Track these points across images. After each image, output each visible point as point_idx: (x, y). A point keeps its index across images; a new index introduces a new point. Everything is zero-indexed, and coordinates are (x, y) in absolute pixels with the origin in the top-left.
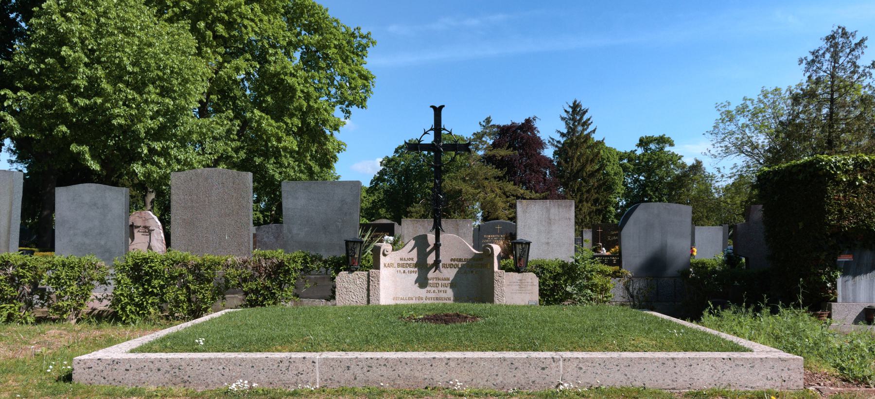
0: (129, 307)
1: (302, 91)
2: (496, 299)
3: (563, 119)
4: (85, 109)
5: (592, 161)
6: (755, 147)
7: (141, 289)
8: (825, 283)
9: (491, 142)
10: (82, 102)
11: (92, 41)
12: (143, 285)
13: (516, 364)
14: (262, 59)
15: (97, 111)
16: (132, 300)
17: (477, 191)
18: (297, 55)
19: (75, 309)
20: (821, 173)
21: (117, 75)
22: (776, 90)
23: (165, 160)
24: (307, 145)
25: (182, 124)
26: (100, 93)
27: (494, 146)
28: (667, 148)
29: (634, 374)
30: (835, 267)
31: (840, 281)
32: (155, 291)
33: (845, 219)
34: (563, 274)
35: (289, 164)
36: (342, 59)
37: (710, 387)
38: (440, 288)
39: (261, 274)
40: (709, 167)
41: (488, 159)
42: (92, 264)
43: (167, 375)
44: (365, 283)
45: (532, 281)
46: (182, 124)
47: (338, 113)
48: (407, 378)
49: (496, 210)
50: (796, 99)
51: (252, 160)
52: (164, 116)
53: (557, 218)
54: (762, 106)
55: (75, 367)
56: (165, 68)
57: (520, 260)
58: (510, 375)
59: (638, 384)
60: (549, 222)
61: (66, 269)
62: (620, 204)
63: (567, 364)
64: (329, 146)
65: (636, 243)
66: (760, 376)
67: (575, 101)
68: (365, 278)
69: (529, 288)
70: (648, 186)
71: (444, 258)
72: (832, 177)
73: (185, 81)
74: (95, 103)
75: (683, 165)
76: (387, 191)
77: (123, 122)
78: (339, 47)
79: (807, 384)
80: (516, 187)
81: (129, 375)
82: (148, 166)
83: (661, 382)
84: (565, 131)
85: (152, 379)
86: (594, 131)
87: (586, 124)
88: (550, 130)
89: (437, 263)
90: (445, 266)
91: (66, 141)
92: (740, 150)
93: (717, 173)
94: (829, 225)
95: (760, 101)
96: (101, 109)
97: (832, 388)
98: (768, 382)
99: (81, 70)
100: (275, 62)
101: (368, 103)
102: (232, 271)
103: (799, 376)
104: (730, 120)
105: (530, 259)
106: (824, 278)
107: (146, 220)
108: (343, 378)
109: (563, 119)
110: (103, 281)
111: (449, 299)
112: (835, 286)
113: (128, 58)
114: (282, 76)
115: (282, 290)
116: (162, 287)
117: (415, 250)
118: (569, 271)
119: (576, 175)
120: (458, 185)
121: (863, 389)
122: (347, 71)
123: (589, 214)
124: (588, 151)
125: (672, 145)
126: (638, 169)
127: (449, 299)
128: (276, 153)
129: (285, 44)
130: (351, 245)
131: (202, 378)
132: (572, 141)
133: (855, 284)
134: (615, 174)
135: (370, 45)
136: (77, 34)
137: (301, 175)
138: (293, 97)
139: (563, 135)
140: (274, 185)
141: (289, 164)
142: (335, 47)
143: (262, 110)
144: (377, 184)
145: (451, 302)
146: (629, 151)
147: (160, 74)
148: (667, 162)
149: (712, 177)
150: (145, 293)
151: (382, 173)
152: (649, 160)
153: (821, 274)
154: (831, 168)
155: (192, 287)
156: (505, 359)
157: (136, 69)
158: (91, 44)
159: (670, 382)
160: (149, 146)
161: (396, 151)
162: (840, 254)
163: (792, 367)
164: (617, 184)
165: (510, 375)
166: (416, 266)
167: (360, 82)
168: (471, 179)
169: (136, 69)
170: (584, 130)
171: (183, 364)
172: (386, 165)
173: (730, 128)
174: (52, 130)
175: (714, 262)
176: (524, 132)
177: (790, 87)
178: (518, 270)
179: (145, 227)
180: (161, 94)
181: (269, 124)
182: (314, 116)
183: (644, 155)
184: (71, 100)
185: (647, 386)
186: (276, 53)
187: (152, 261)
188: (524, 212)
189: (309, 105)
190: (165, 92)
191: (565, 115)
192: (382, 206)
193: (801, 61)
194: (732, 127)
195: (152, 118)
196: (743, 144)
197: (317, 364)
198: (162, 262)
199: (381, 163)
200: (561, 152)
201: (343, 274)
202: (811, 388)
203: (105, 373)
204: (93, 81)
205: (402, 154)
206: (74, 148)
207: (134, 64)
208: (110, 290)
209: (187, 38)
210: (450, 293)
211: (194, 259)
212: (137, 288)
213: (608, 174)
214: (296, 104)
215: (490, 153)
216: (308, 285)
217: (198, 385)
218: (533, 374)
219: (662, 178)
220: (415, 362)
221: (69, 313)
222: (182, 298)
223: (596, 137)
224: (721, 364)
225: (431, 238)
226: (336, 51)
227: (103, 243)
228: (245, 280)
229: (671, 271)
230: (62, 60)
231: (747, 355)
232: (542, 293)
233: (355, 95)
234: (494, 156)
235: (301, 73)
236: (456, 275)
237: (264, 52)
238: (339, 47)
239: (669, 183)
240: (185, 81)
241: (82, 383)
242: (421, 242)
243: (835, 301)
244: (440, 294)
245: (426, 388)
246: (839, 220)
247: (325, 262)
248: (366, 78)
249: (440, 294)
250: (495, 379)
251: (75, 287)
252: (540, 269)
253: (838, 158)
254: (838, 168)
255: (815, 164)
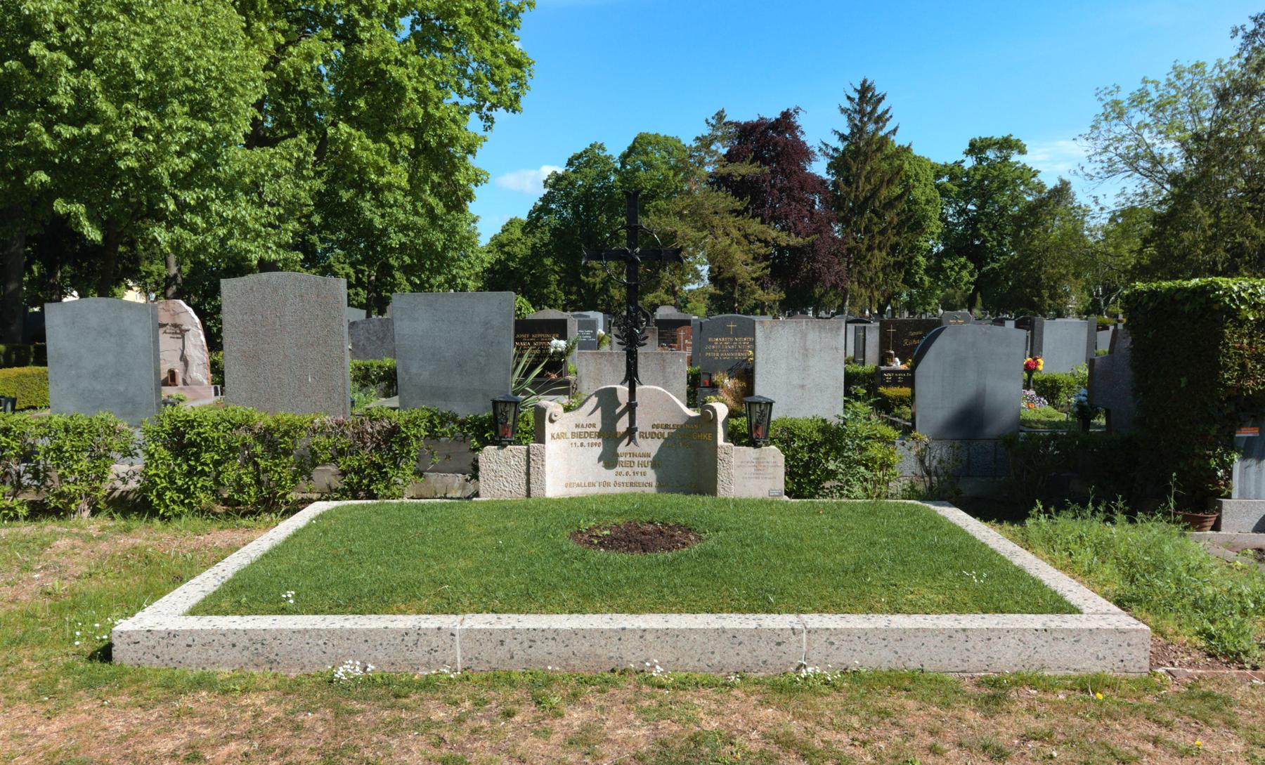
0: (168, 494)
1: (416, 90)
2: (719, 487)
3: (844, 111)
4: (73, 142)
5: (890, 182)
6: (1156, 161)
7: (185, 467)
8: (1215, 470)
9: (724, 151)
10: (67, 131)
11: (77, 28)
12: (187, 460)
13: (741, 638)
14: (348, 34)
15: (92, 145)
16: (172, 482)
17: (701, 235)
18: (405, 23)
19: (87, 495)
20: (1216, 307)
21: (120, 86)
22: (1197, 66)
23: (203, 218)
24: (426, 172)
25: (227, 161)
26: (93, 115)
27: (730, 157)
28: (1015, 158)
29: (908, 652)
30: (1231, 446)
31: (1237, 467)
32: (207, 469)
33: (1248, 377)
34: (822, 444)
35: (396, 201)
36: (479, 32)
37: (1015, 669)
38: (636, 469)
39: (365, 443)
40: (1081, 195)
41: (719, 181)
42: (108, 427)
43: (245, 653)
44: (523, 463)
45: (774, 456)
46: (227, 161)
47: (474, 124)
48: (585, 657)
49: (732, 265)
50: (1223, 97)
51: (337, 194)
52: (198, 149)
53: (818, 347)
54: (1173, 92)
55: (115, 642)
56: (196, 72)
57: (757, 428)
58: (732, 652)
59: (914, 665)
60: (806, 353)
61: (71, 436)
62: (935, 250)
63: (813, 637)
64: (460, 177)
65: (939, 388)
66: (1088, 654)
67: (865, 81)
68: (523, 456)
69: (771, 470)
70: (981, 221)
71: (642, 424)
72: (1233, 314)
73: (230, 92)
74: (89, 133)
75: (1041, 187)
76: (556, 229)
77: (136, 165)
78: (474, 13)
79: (1154, 665)
80: (764, 227)
81: (192, 653)
82: (177, 229)
83: (946, 662)
84: (847, 132)
85: (224, 658)
86: (894, 131)
87: (881, 120)
88: (822, 130)
89: (631, 432)
90: (643, 435)
91: (48, 194)
92: (1132, 162)
93: (1093, 206)
94: (1224, 386)
95: (1170, 84)
96: (94, 143)
97: (1189, 671)
98: (1098, 663)
99: (63, 79)
100: (370, 41)
101: (523, 102)
102: (322, 440)
103: (1143, 654)
104: (1120, 116)
105: (773, 418)
106: (1213, 463)
107: (176, 314)
108: (494, 657)
109: (844, 111)
110: (127, 453)
111: (650, 485)
112: (1229, 474)
113: (137, 59)
114: (383, 66)
115: (397, 467)
116: (217, 463)
117: (599, 412)
118: (832, 438)
119: (860, 208)
120: (669, 224)
121: (1234, 671)
122: (487, 54)
123: (884, 269)
124: (885, 166)
125: (1022, 151)
126: (966, 192)
127: (650, 485)
128: (377, 190)
129: (386, 9)
130: (500, 407)
131: (295, 657)
132: (858, 147)
133: (1260, 471)
134: (928, 202)
135: (526, 7)
136: (52, 18)
137: (416, 218)
138: (399, 100)
139: (843, 137)
140: (373, 235)
141: (396, 201)
142: (468, 12)
143: (349, 121)
144: (538, 218)
145: (653, 490)
146: (950, 162)
147: (190, 83)
148: (1013, 181)
149: (1086, 212)
150: (190, 473)
151: (546, 199)
152: (984, 177)
153: (1210, 457)
154: (1232, 300)
155: (262, 463)
156: (724, 631)
157: (151, 76)
158: (75, 34)
159: (959, 662)
160: (175, 197)
161: (570, 163)
162: (1241, 426)
163: (1134, 641)
164: (930, 218)
165: (732, 652)
166: (599, 435)
167: (508, 71)
168: (692, 213)
169: (151, 76)
170: (877, 130)
171: (267, 637)
172: (553, 186)
173: (1117, 130)
174: (22, 178)
175: (1071, 379)
176: (780, 133)
177: (1220, 61)
178: (754, 443)
179: (175, 326)
180: (193, 114)
181: (361, 145)
182: (435, 130)
183: (975, 169)
184: (49, 129)
185: (926, 668)
186: (372, 25)
187: (200, 425)
188: (767, 338)
189: (426, 111)
190: (199, 110)
191: (847, 104)
192: (548, 254)
193: (1235, 32)
194: (1121, 129)
195: (179, 154)
196: (1137, 157)
197: (457, 638)
198: (215, 426)
199: (545, 182)
200: (839, 164)
201: (490, 449)
202: (1161, 670)
203: (158, 650)
204: (80, 93)
205: (578, 167)
206: (60, 206)
207: (145, 68)
208: (139, 465)
209: (228, 18)
210: (651, 476)
211: (263, 419)
212: (180, 466)
213: (915, 202)
214: (405, 112)
215: (722, 170)
216: (437, 460)
217: (290, 666)
218: (764, 651)
219: (1003, 209)
220: (597, 635)
221: (79, 501)
222: (247, 479)
223: (899, 140)
224: (1033, 637)
225: (623, 391)
226: (469, 19)
227: (122, 389)
228: (341, 452)
229: (992, 430)
230: (30, 62)
231: (1071, 622)
232: (790, 474)
233: (503, 86)
234: (730, 175)
235: (412, 59)
236: (660, 450)
237: (351, 22)
238: (474, 13)
239: (1014, 217)
240: (230, 92)
241: (127, 663)
242: (607, 399)
243: (1229, 496)
244: (635, 479)
245: (613, 671)
246: (1239, 379)
247: (462, 424)
248: (519, 65)
249: (635, 479)
250: (709, 659)
251: (84, 464)
252: (787, 438)
253: (1245, 284)
254: (1242, 300)
255: (1209, 292)
